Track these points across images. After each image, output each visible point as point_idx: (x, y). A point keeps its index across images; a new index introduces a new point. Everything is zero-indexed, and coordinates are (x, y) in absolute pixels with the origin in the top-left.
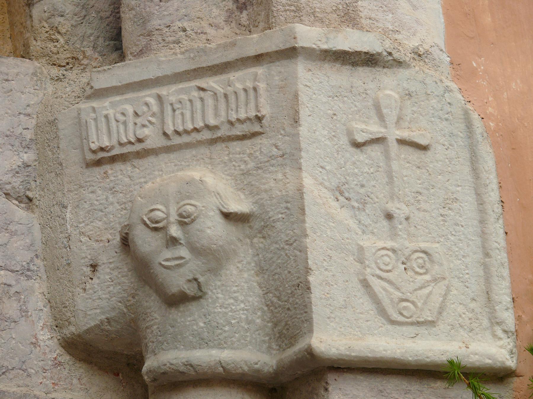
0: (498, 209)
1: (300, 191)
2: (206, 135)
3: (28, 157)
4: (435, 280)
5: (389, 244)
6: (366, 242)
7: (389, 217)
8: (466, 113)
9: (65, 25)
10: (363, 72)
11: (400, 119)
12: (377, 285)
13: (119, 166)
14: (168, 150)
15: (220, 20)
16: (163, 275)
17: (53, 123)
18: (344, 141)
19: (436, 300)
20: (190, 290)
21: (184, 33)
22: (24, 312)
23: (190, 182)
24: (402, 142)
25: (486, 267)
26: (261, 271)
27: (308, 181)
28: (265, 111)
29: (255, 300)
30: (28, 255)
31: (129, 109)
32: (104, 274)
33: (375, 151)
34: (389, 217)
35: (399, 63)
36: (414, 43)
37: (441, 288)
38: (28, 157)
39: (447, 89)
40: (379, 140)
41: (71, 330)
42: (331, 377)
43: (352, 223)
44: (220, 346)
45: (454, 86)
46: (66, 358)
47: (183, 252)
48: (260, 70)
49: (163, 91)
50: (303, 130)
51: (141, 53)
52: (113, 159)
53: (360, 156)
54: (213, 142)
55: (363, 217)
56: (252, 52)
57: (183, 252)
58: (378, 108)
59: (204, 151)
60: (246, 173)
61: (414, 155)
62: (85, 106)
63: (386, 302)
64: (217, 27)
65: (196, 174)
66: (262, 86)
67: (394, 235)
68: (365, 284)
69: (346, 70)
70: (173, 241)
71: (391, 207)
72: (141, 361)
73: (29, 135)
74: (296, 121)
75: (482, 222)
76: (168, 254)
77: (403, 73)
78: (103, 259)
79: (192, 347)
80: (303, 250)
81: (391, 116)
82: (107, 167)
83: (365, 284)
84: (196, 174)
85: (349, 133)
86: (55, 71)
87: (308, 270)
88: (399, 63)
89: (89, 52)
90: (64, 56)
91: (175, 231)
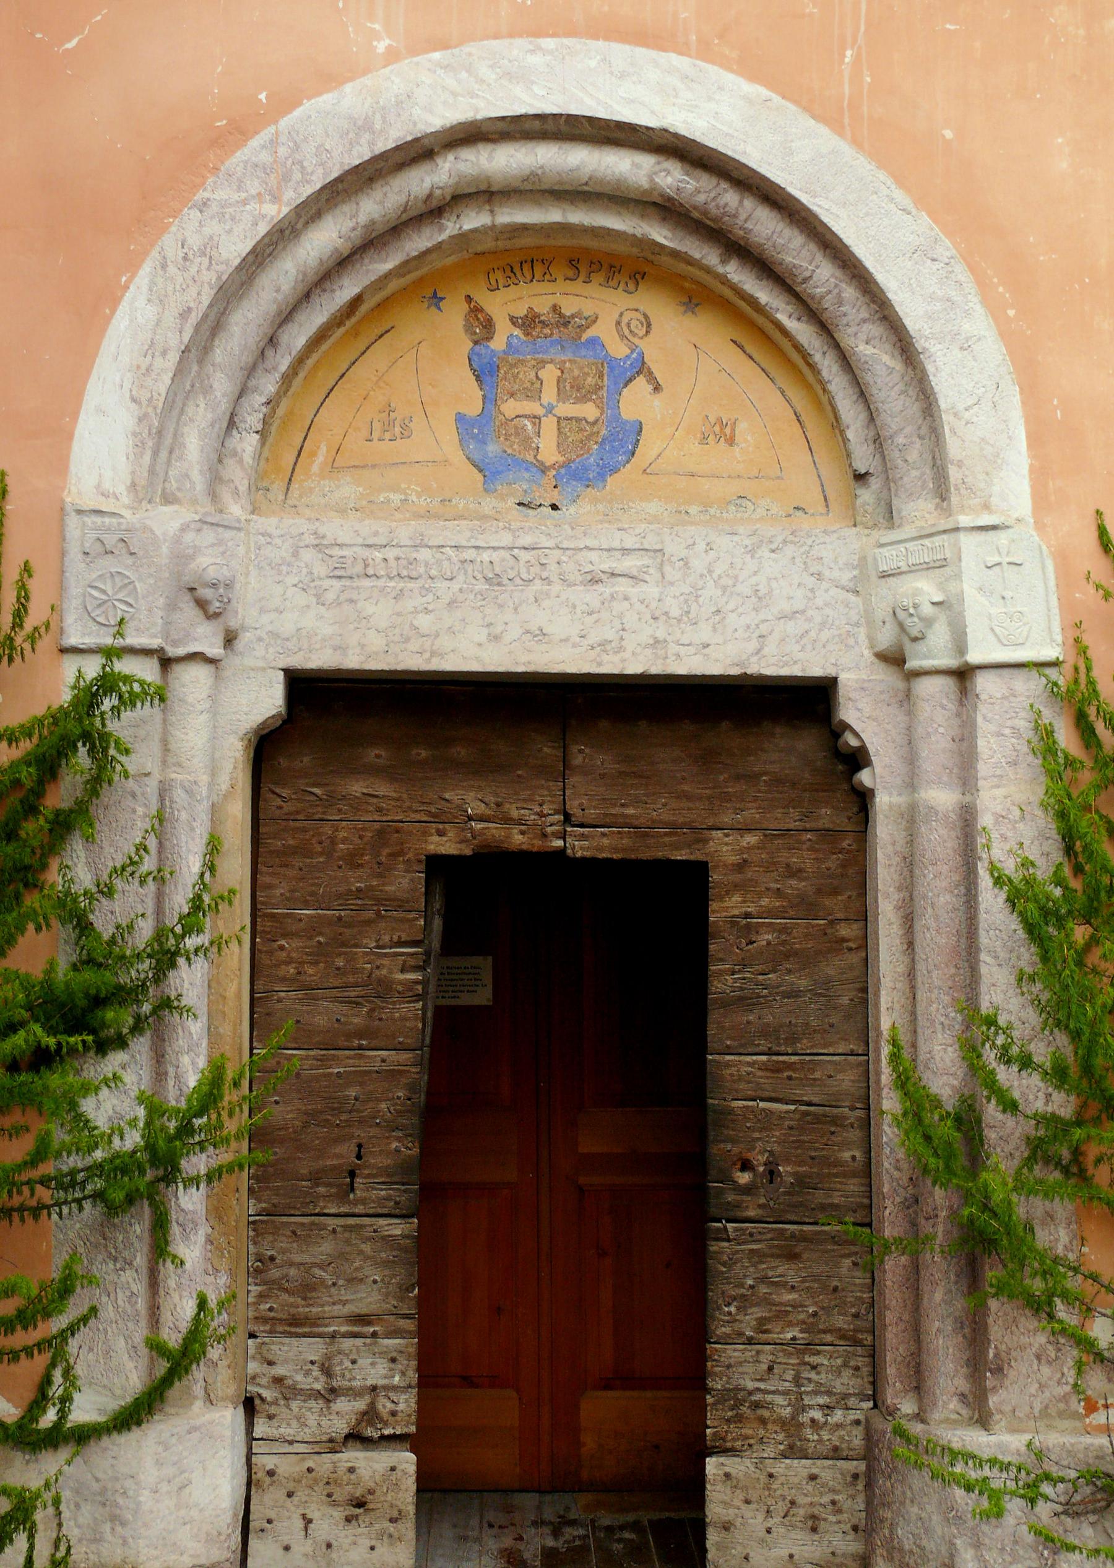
0: (1054, 589)
1: (962, 592)
2: (925, 566)
3: (855, 572)
4: (1025, 624)
5: (1004, 610)
6: (993, 611)
7: (1003, 598)
8: (1040, 546)
9: (869, 509)
10: (991, 533)
11: (1008, 553)
12: (998, 630)
13: (891, 578)
14: (910, 572)
15: (933, 510)
16: (908, 629)
17: (865, 558)
18: (983, 566)
19: (1025, 633)
20: (919, 635)
21: (335, 1384)
22: (857, 643)
23: (917, 589)
24: (1009, 563)
25: (1049, 616)
26: (949, 624)
27: (965, 586)
28: (948, 555)
29: (947, 637)
30: (857, 617)
31: (894, 553)
32: (887, 624)
33: (997, 569)
34: (1003, 598)
35: (1008, 527)
36: (1016, 515)
37: (1027, 627)
38: (855, 572)
39: (1032, 536)
40: (999, 564)
41: (877, 649)
42: (978, 671)
43: (987, 603)
44: (933, 658)
45: (1034, 533)
46: (876, 661)
47: (916, 619)
48: (945, 536)
49: (908, 545)
50: (963, 564)
51: (899, 527)
52: (889, 576)
53: (990, 572)
54: (928, 569)
55: (992, 599)
56: (942, 528)
57: (916, 619)
58: (998, 549)
59: (924, 572)
60: (941, 583)
61: (1015, 568)
62: (877, 551)
63: (1001, 637)
64: (930, 513)
65: (919, 585)
66: (946, 544)
67: (1005, 606)
68: (992, 630)
69: (984, 533)
70: (911, 615)
71: (1004, 594)
72: (905, 662)
73: (855, 563)
74: (960, 560)
75: (1047, 595)
76: (910, 620)
77: (1010, 531)
78: (887, 619)
79: (921, 659)
80: (964, 617)
81: (1004, 551)
82: (887, 579)
83: (992, 630)
84: (919, 585)
85: (985, 562)
86: (867, 531)
87: (966, 626)
88: (1008, 527)
89: (881, 520)
90: (870, 524)
91: (912, 611)
